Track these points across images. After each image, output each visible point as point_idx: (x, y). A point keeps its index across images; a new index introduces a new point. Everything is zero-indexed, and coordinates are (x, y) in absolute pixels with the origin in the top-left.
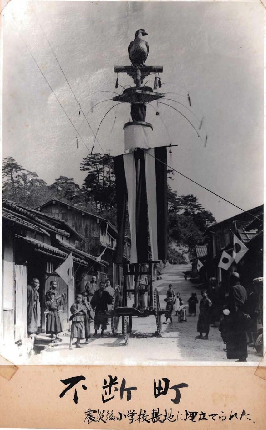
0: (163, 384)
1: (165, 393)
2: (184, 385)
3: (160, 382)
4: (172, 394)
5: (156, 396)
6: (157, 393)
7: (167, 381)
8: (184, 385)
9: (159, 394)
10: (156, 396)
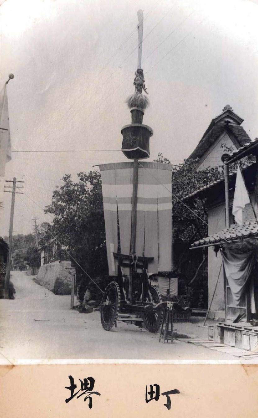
1: (157, 398)
2: (175, 392)
4: (163, 399)
5: (147, 401)
6: (149, 398)
8: (175, 392)
9: (152, 399)
10: (147, 401)
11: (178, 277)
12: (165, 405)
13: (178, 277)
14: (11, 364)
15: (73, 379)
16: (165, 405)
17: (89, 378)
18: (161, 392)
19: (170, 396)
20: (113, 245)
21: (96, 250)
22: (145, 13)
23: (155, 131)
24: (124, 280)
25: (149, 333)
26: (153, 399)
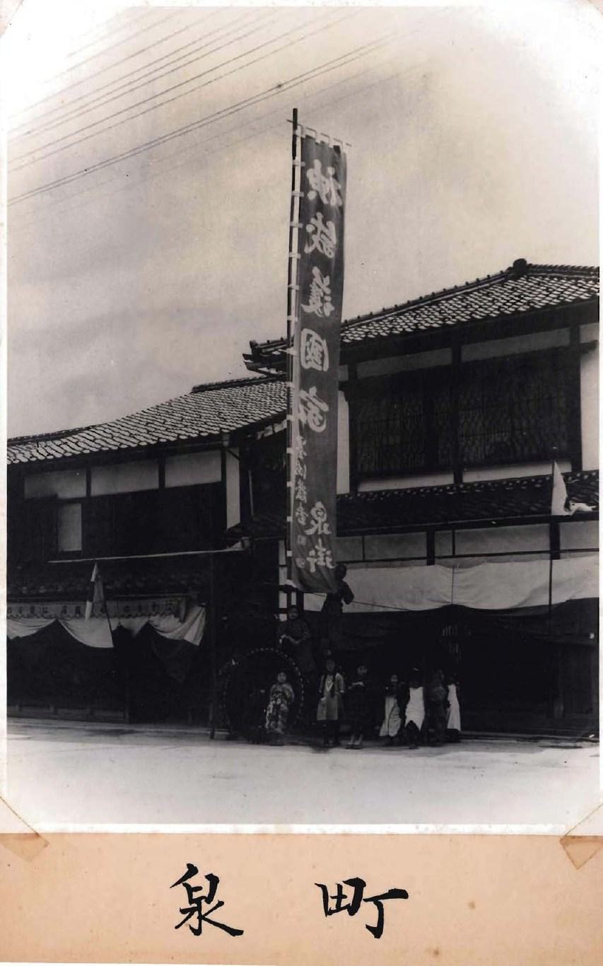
0: (349, 891)
1: (353, 909)
3: (340, 887)
4: (368, 912)
5: (328, 912)
7: (358, 884)
9: (339, 908)
10: (328, 912)
11: (343, 602)
12: (368, 927)
13: (343, 602)
14: (32, 832)
15: (395, 889)
16: (368, 927)
17: (349, 882)
18: (367, 893)
19: (384, 902)
20: (320, 610)
21: (281, 641)
22: (13, 436)
23: (477, 277)
24: (457, 646)
25: (311, 754)
26: (344, 908)
